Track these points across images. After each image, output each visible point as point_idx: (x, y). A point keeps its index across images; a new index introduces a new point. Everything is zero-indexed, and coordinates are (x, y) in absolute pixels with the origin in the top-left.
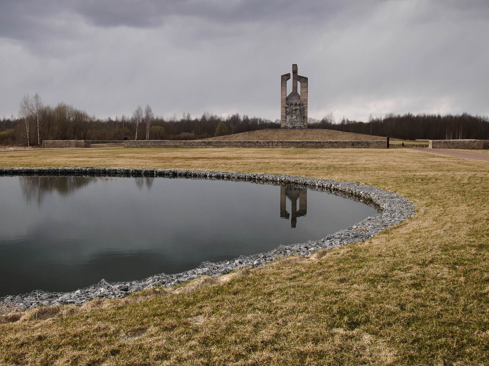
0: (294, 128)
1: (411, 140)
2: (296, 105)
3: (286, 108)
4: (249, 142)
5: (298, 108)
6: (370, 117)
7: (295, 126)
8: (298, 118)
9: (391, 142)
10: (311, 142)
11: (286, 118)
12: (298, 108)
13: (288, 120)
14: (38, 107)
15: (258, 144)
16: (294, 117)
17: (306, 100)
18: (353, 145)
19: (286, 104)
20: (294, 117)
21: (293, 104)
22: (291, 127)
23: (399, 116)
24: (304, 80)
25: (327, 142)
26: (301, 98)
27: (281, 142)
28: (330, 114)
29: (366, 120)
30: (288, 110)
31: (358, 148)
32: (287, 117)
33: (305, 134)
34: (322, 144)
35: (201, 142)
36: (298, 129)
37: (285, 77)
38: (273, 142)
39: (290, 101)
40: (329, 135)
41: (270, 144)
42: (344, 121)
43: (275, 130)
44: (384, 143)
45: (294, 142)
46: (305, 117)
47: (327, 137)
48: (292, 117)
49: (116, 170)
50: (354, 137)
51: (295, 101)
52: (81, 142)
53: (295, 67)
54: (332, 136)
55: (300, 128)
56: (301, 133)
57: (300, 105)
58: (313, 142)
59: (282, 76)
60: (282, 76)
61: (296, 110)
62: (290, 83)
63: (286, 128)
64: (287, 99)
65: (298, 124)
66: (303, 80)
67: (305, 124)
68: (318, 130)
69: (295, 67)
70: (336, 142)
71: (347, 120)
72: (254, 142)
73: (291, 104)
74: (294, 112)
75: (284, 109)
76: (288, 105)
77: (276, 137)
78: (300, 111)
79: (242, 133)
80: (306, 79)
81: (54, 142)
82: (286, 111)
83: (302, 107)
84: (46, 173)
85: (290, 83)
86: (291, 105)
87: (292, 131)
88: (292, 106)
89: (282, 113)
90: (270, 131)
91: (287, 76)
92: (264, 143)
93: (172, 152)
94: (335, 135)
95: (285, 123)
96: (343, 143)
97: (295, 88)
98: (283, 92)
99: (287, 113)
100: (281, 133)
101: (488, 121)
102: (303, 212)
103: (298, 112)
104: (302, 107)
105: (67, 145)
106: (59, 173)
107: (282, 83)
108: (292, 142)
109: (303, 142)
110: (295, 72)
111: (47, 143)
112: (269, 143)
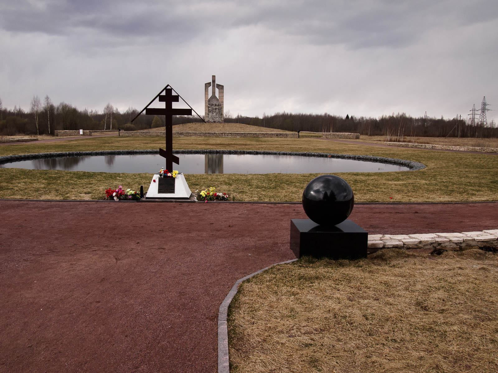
0: (214, 122)
1: (289, 131)
2: (216, 105)
3: (209, 107)
4: (209, 133)
5: (217, 107)
6: (264, 115)
7: (215, 120)
8: (217, 115)
9: (300, 134)
10: (250, 134)
11: (209, 115)
12: (217, 107)
13: (210, 116)
14: (133, 109)
15: (215, 134)
16: (215, 114)
17: (223, 102)
18: (277, 136)
19: (209, 104)
20: (215, 114)
21: (213, 105)
22: (212, 121)
23: (347, 116)
24: (221, 87)
25: (261, 134)
26: (219, 100)
27: (231, 133)
28: (228, 111)
29: (261, 117)
30: (210, 109)
31: (280, 138)
32: (210, 114)
33: (223, 126)
34: (258, 135)
35: (175, 133)
36: (217, 123)
37: (207, 85)
38: (225, 133)
39: (211, 103)
40: (241, 128)
41: (223, 135)
42: (238, 116)
43: (202, 123)
44: (297, 134)
45: (239, 133)
46: (222, 114)
47: (240, 129)
48: (213, 114)
49: (223, 151)
50: (258, 129)
51: (215, 102)
52: (87, 132)
53: (214, 77)
54: (242, 128)
55: (219, 122)
56: (221, 125)
57: (218, 105)
58: (251, 134)
59: (205, 84)
60: (205, 84)
61: (216, 109)
62: (210, 89)
63: (208, 122)
64: (209, 101)
65: (217, 119)
66: (220, 87)
67: (222, 120)
68: (232, 124)
69: (214, 77)
70: (266, 134)
71: (241, 116)
72: (213, 133)
73: (212, 105)
74: (214, 110)
75: (207, 108)
76: (210, 105)
77: (203, 129)
78: (219, 110)
79: (178, 125)
80: (223, 86)
81: (66, 131)
82: (209, 110)
83: (220, 107)
84: (186, 152)
85: (210, 89)
86: (212, 105)
87: (215, 124)
88: (213, 106)
89: (205, 111)
90: (198, 124)
91: (209, 84)
92: (219, 134)
93: (455, 139)
94: (245, 128)
95: (208, 119)
96: (270, 134)
97: (214, 93)
98: (206, 95)
99: (209, 111)
100: (206, 125)
101: (496, 126)
102: (207, 85)
103: (217, 111)
104: (220, 107)
105: (76, 134)
106: (193, 152)
107: (205, 89)
108: (238, 133)
109: (245, 133)
110: (214, 81)
111: (60, 132)
112: (222, 134)
